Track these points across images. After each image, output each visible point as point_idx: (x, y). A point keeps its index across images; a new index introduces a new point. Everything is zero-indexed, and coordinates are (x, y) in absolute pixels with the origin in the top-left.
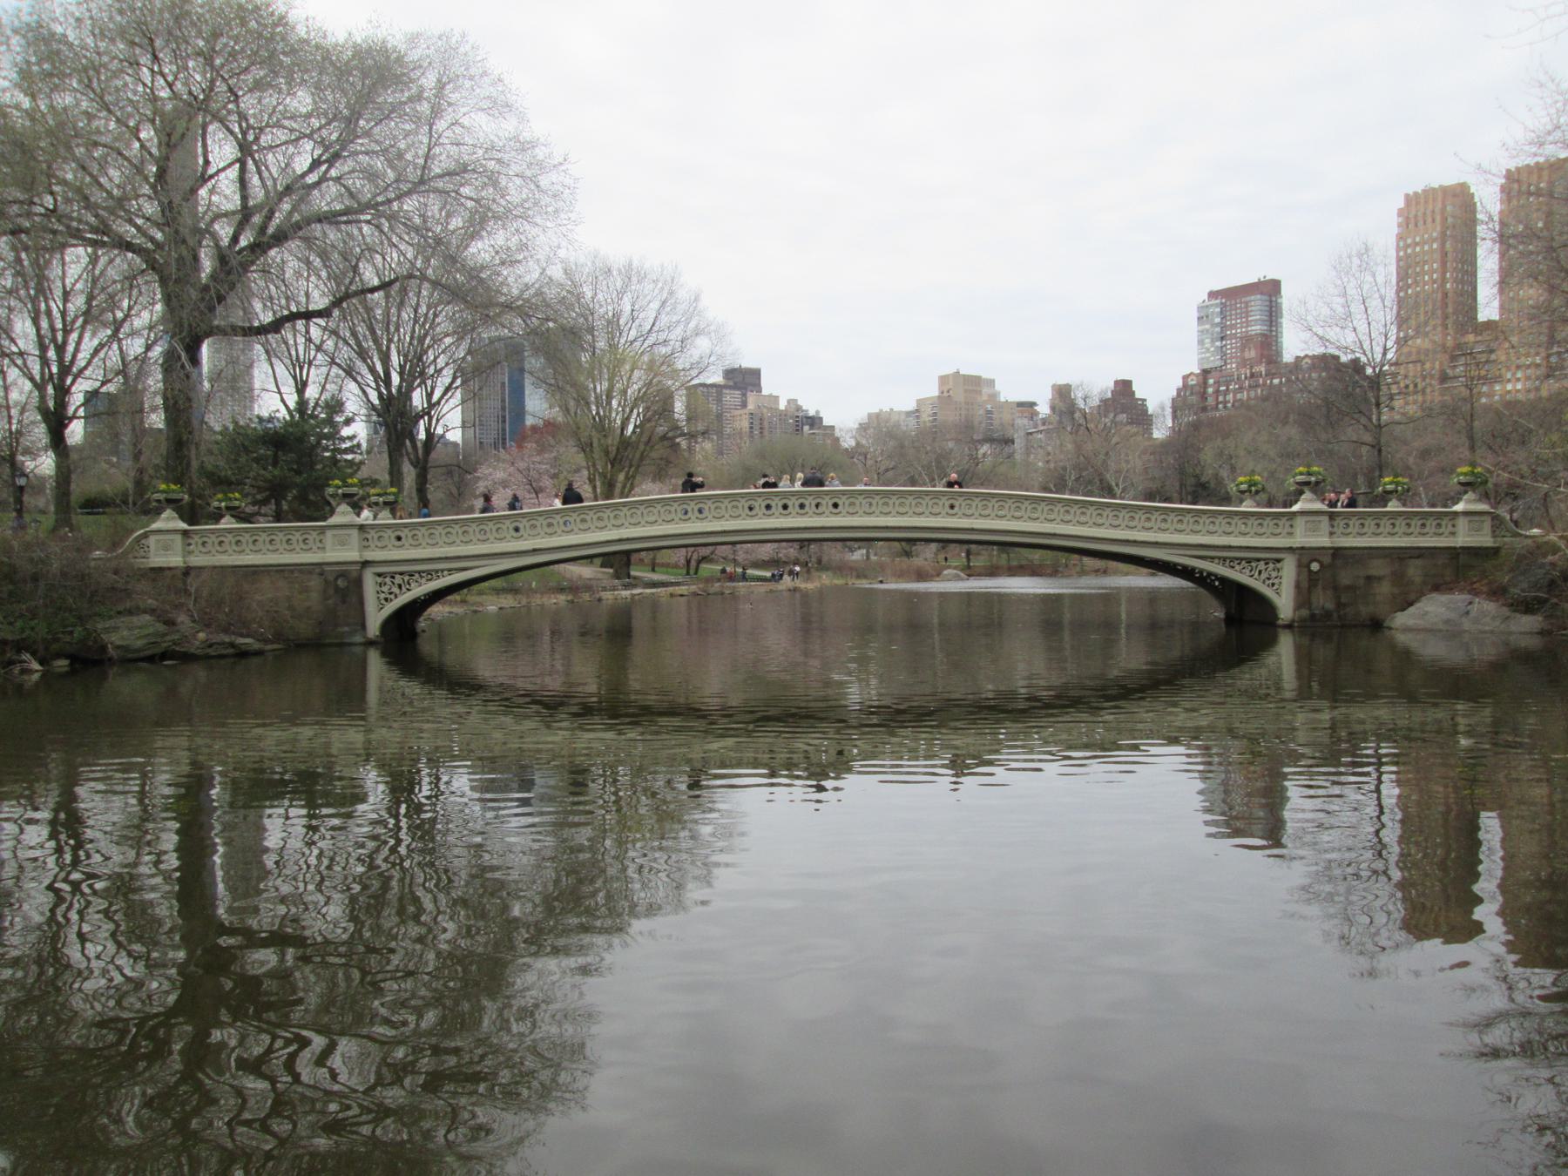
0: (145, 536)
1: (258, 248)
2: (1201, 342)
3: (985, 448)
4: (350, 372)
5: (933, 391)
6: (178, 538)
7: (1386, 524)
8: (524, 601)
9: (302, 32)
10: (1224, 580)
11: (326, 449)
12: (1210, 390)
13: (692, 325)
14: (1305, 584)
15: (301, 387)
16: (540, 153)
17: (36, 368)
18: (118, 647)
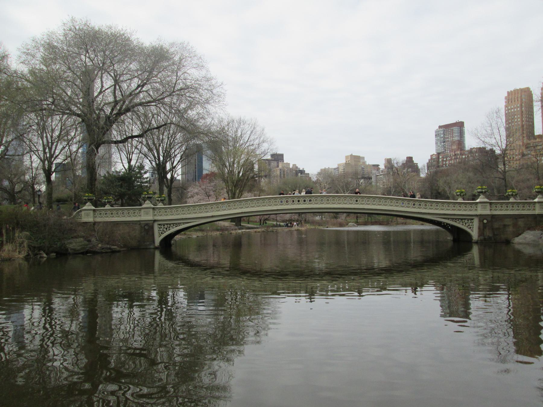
0: (81, 211)
1: (120, 114)
2: (436, 143)
3: (362, 181)
4: (146, 156)
5: (343, 161)
6: (92, 212)
7: (510, 206)
8: (205, 234)
9: (135, 43)
10: (452, 226)
11: (138, 182)
12: (440, 160)
13: (262, 139)
14: (482, 228)
15: (129, 161)
16: (213, 82)
17: (42, 156)
18: (72, 249)
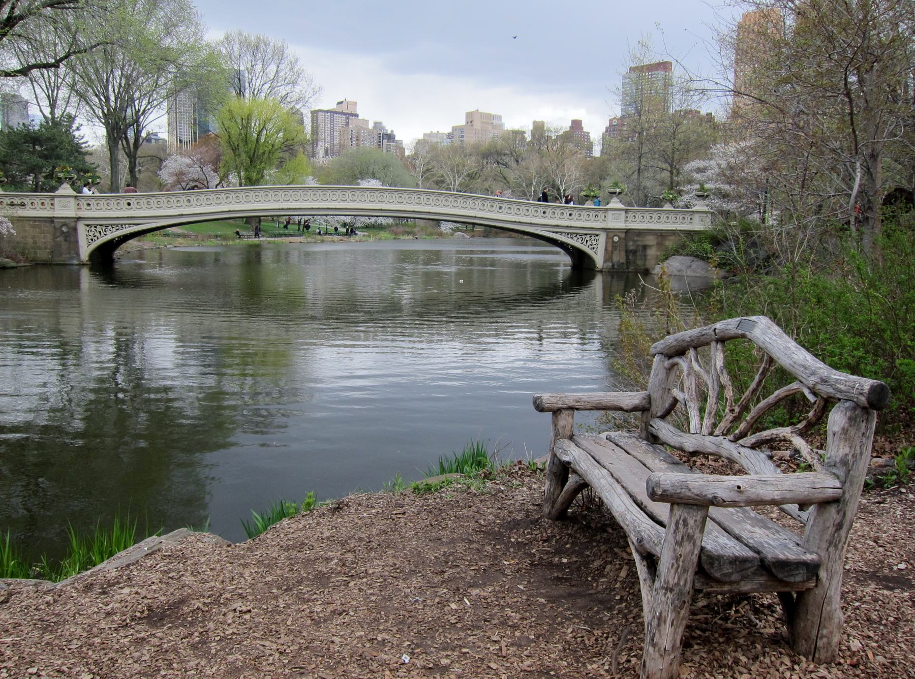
14: (610, 249)
15: (53, 106)
